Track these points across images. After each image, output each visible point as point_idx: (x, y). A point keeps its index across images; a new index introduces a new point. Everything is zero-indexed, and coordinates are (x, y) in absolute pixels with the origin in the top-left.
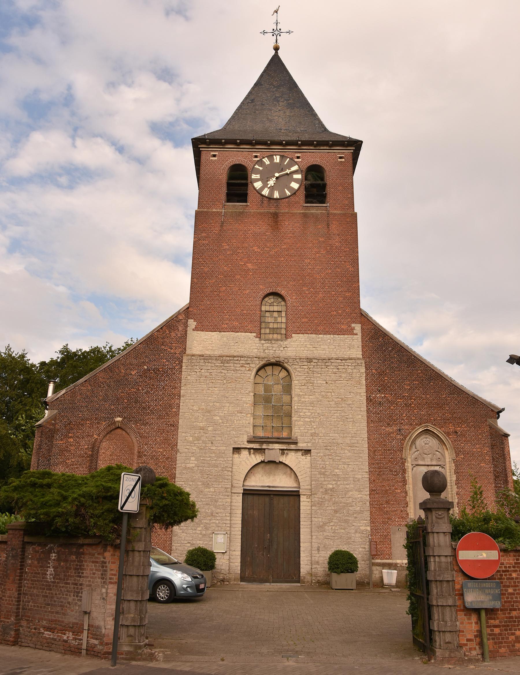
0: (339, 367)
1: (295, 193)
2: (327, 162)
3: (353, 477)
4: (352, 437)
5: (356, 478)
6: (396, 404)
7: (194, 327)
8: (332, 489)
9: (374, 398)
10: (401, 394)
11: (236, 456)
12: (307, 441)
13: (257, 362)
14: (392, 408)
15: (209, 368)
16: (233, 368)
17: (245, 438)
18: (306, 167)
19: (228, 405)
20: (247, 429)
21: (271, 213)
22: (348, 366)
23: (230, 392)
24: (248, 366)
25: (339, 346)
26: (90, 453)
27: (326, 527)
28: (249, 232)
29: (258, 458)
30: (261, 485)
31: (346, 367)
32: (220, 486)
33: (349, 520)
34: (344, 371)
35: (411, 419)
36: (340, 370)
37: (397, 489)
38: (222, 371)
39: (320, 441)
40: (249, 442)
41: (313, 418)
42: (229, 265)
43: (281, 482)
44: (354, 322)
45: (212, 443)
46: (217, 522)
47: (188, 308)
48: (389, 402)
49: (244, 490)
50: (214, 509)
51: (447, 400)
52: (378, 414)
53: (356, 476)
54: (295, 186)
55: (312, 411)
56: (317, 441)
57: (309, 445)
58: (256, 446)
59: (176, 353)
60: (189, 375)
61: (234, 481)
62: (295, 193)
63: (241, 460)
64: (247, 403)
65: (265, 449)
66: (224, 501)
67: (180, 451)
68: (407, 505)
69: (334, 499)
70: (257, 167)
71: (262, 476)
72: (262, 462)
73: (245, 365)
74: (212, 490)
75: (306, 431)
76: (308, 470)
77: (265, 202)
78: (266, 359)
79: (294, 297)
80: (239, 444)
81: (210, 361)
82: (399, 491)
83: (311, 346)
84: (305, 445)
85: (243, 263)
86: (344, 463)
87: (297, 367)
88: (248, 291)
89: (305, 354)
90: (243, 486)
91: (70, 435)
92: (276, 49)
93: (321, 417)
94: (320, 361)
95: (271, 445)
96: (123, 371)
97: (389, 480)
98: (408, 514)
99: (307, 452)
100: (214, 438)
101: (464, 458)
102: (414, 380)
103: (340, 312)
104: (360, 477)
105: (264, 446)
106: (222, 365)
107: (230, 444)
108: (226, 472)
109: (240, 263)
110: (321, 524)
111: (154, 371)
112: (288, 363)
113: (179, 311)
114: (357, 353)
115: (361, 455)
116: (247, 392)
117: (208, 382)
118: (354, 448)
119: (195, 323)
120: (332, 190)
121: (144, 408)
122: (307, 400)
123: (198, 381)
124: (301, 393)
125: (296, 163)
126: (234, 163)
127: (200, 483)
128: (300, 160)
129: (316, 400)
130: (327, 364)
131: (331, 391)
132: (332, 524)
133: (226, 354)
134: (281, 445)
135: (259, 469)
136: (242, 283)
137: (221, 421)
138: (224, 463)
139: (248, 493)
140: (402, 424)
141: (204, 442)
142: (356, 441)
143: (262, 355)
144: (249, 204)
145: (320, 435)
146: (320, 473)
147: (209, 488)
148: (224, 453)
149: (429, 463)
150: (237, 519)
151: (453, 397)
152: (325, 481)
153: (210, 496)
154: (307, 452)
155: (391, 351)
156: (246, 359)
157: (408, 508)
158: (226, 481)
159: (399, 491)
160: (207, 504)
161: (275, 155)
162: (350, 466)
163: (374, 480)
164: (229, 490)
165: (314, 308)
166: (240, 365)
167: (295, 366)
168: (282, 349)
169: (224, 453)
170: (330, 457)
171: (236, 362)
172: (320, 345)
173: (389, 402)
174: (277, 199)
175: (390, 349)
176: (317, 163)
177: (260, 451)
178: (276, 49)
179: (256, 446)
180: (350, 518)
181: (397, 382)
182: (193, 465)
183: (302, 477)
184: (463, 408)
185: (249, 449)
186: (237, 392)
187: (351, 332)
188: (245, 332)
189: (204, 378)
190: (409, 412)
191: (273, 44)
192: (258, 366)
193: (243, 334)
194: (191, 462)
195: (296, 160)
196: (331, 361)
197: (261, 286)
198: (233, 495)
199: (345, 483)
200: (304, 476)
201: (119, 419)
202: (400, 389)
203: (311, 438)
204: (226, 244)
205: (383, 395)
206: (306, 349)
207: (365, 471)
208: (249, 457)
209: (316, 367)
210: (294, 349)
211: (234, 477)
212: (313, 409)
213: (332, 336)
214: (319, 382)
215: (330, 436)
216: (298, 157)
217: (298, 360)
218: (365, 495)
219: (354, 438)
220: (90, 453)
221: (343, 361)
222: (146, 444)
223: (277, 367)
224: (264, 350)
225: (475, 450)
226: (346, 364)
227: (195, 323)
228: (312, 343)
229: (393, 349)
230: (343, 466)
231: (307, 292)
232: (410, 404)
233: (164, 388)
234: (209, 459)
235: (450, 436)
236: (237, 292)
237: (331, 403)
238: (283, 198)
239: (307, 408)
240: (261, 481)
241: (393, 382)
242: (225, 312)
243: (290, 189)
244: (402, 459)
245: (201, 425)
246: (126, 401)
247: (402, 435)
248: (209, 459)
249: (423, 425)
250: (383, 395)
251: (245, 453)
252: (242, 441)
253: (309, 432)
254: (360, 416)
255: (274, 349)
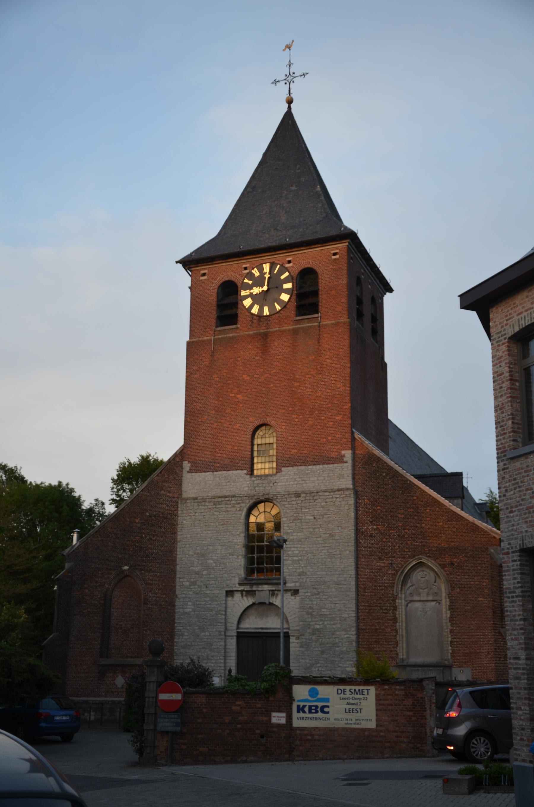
0: (328, 500)
1: (285, 306)
2: (320, 262)
3: (340, 617)
4: (340, 574)
5: (343, 617)
6: (389, 536)
7: (188, 469)
8: (318, 630)
9: (366, 530)
10: (394, 524)
11: (230, 599)
12: (295, 581)
13: (247, 501)
14: (384, 540)
15: (203, 511)
16: (224, 509)
17: (237, 580)
18: (297, 272)
19: (220, 547)
20: (239, 572)
21: (260, 334)
22: (337, 498)
23: (222, 534)
24: (238, 506)
25: (328, 476)
26: (102, 602)
27: (313, 669)
28: (239, 359)
29: (248, 601)
30: (255, 627)
31: (334, 499)
32: (215, 630)
33: (335, 661)
34: (332, 503)
35: (404, 551)
36: (328, 503)
37: (386, 627)
38: (215, 513)
39: (308, 580)
40: (240, 584)
41: (301, 556)
42: (220, 399)
43: (271, 623)
44: (344, 449)
45: (207, 587)
46: (213, 665)
47: (183, 450)
48: (382, 533)
49: (238, 632)
50: (209, 653)
51: (443, 528)
52: (370, 547)
53: (343, 616)
54: (285, 297)
55: (300, 549)
56: (304, 581)
57: (297, 584)
58: (247, 588)
59: (174, 498)
60: (185, 520)
61: (228, 624)
62: (285, 307)
63: (234, 602)
64: (238, 545)
65: (255, 591)
66: (218, 644)
67: (179, 596)
68: (397, 644)
69: (321, 640)
70: (246, 281)
71: (256, 618)
72: (254, 604)
73: (236, 506)
74: (207, 634)
75: (294, 570)
76: (297, 610)
77: (255, 321)
78: (256, 497)
79: (283, 427)
80: (232, 587)
81: (203, 503)
82: (389, 630)
83: (300, 480)
84: (293, 585)
85: (233, 395)
86: (331, 602)
87: (285, 503)
88: (238, 425)
89: (295, 487)
90: (238, 628)
91: (85, 586)
92: (290, 101)
93: (309, 555)
94: (308, 495)
95: (260, 586)
96: (128, 520)
97: (379, 619)
98: (397, 654)
99: (295, 592)
100: (208, 582)
101: (460, 593)
102: (408, 508)
103: (330, 438)
104: (346, 616)
105: (254, 588)
106: (214, 506)
107: (223, 588)
108: (219, 615)
109: (231, 395)
110: (308, 665)
111: (155, 517)
112: (277, 500)
113: (176, 453)
114: (348, 483)
115: (348, 593)
116: (238, 533)
117: (201, 525)
118: (341, 586)
119: (189, 465)
120: (325, 296)
121: (148, 555)
122: (295, 537)
123: (193, 525)
124: (289, 531)
125: (287, 270)
126: (223, 280)
127: (197, 628)
128: (291, 265)
129: (303, 537)
130: (315, 498)
131: (319, 526)
132: (318, 665)
133: (219, 495)
134: (270, 586)
135: (252, 611)
136: (232, 417)
137: (214, 565)
138: (218, 606)
139: (243, 637)
140: (394, 557)
141: (200, 587)
142: (343, 579)
143: (253, 492)
144: (239, 326)
145: (308, 573)
146: (308, 613)
147: (205, 632)
148: (217, 597)
149: (425, 599)
150: (231, 661)
151: (451, 525)
152: (312, 621)
153: (206, 640)
154: (295, 592)
155: (385, 477)
156: (236, 499)
157: (398, 648)
158: (220, 624)
159: (389, 630)
160: (204, 648)
161: (265, 263)
162: (337, 605)
163: (364, 619)
164: (223, 633)
165: (303, 437)
166: (230, 506)
167: (283, 503)
168: (271, 484)
169: (217, 597)
170: (317, 596)
171: (228, 502)
172: (309, 477)
173: (382, 533)
174: (267, 316)
175: (384, 474)
176: (309, 266)
177: (251, 593)
178: (290, 101)
179: (247, 588)
180: (336, 659)
181: (391, 511)
182: (190, 610)
183: (292, 618)
184: (462, 536)
185: (242, 591)
186: (228, 533)
187: (340, 460)
188: (236, 470)
189: (198, 522)
190: (402, 544)
191: (285, 96)
192: (248, 505)
193: (235, 472)
194: (188, 607)
195: (287, 265)
196: (320, 494)
197: (251, 419)
198: (227, 638)
199: (332, 622)
200: (294, 616)
201: (126, 568)
202: (394, 519)
203: (299, 577)
204: (216, 376)
205: (375, 527)
206: (296, 483)
207: (352, 609)
208: (241, 600)
209: (304, 502)
210: (284, 484)
211: (229, 620)
212: (301, 547)
213: (321, 466)
214: (307, 517)
215: (317, 575)
216: (289, 262)
217: (286, 496)
218: (352, 635)
219: (341, 576)
220: (102, 602)
221: (332, 494)
222: (151, 591)
223: (269, 503)
224: (255, 487)
225: (472, 583)
226: (334, 496)
227: (189, 465)
228: (301, 476)
229: (387, 474)
230: (330, 605)
231: (297, 420)
232: (404, 535)
233: (164, 534)
234: (204, 603)
235: (446, 569)
236: (228, 427)
237: (318, 539)
238: (273, 313)
239: (296, 546)
240: (253, 624)
241: (386, 512)
242: (217, 450)
243: (280, 302)
244: (393, 595)
245: (197, 569)
246: (131, 549)
247: (394, 569)
248: (204, 603)
249: (417, 557)
250: (375, 527)
251: (238, 596)
252: (234, 584)
253: (298, 571)
254: (348, 552)
255: (264, 485)
